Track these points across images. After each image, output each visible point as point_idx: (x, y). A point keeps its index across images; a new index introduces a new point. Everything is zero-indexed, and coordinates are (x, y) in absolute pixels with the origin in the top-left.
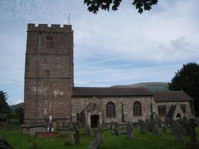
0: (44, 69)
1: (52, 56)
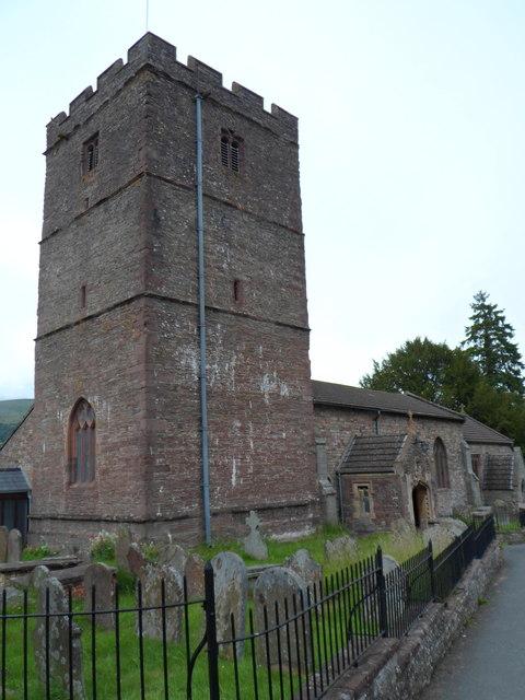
1: (246, 218)
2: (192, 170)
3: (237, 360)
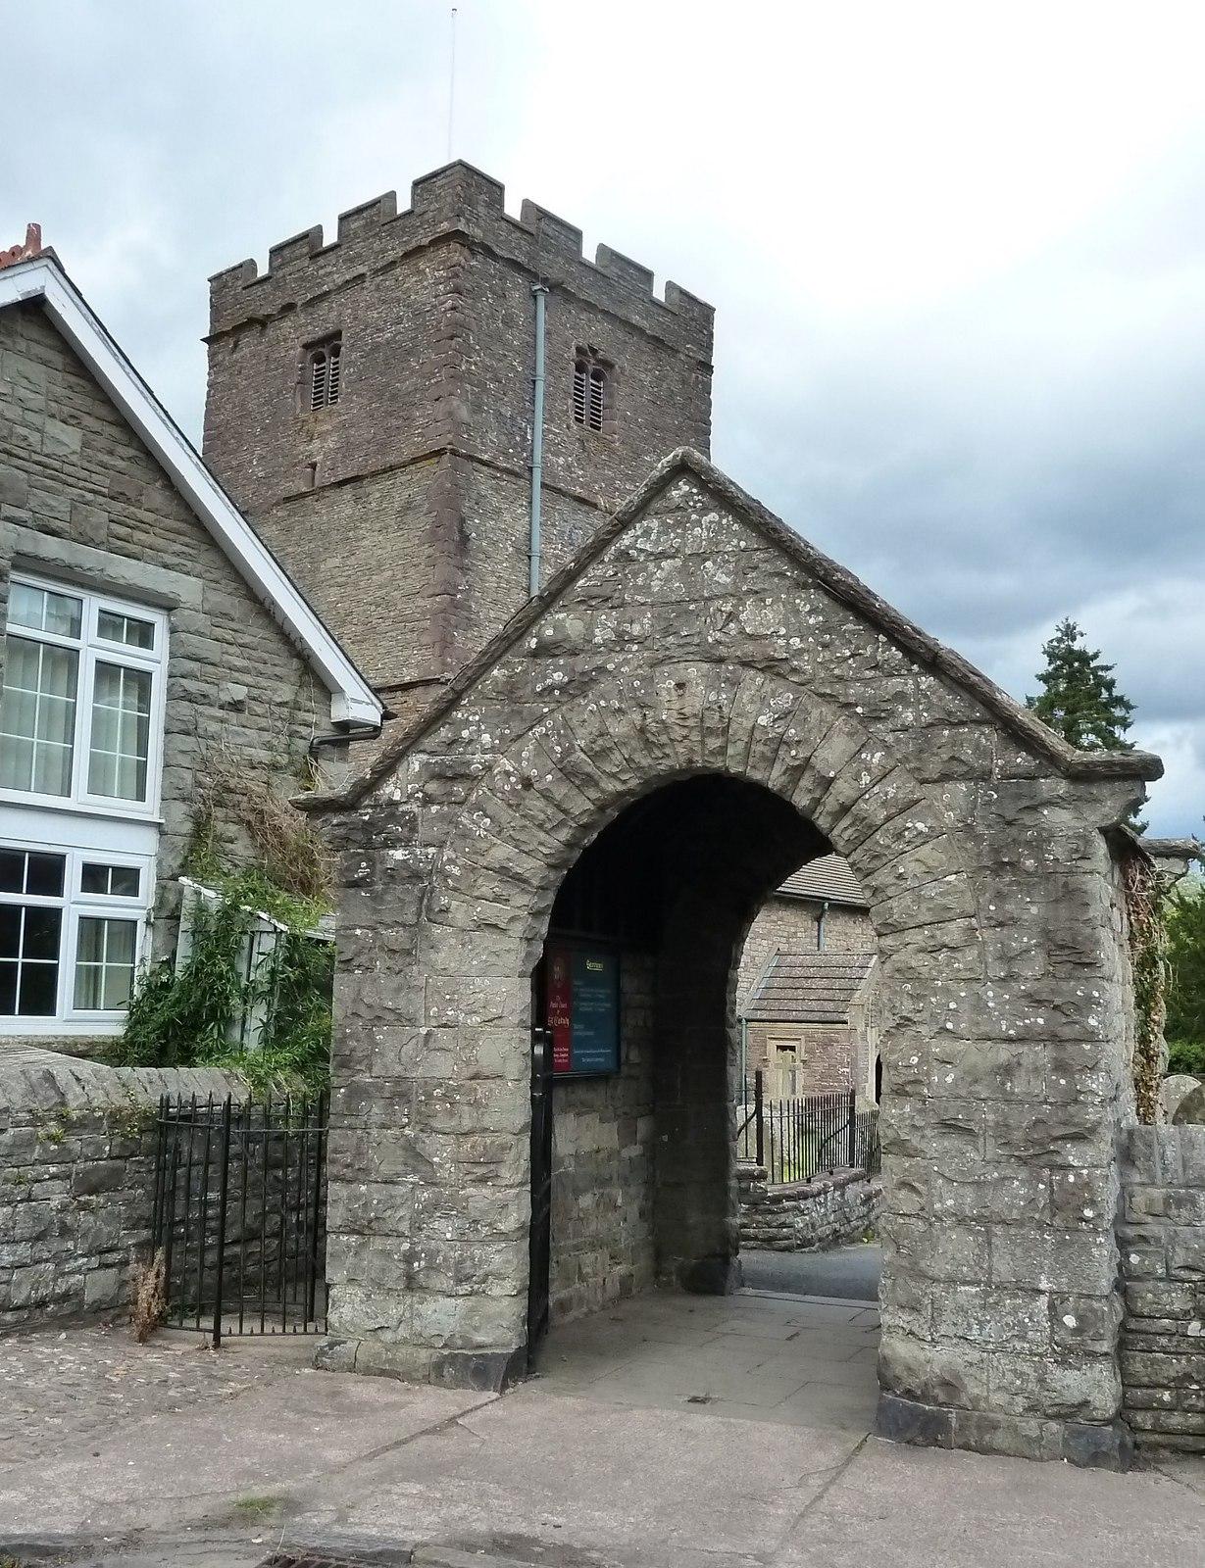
2: (524, 438)
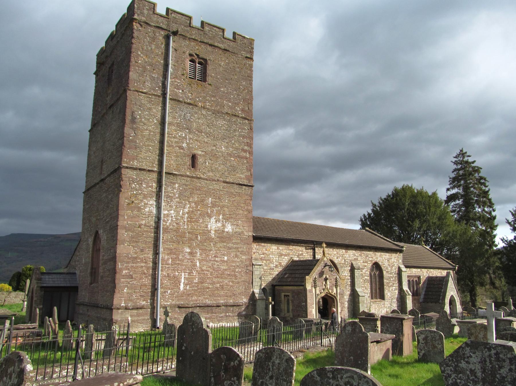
0: (181, 148)
1: (204, 112)
3: (190, 207)
